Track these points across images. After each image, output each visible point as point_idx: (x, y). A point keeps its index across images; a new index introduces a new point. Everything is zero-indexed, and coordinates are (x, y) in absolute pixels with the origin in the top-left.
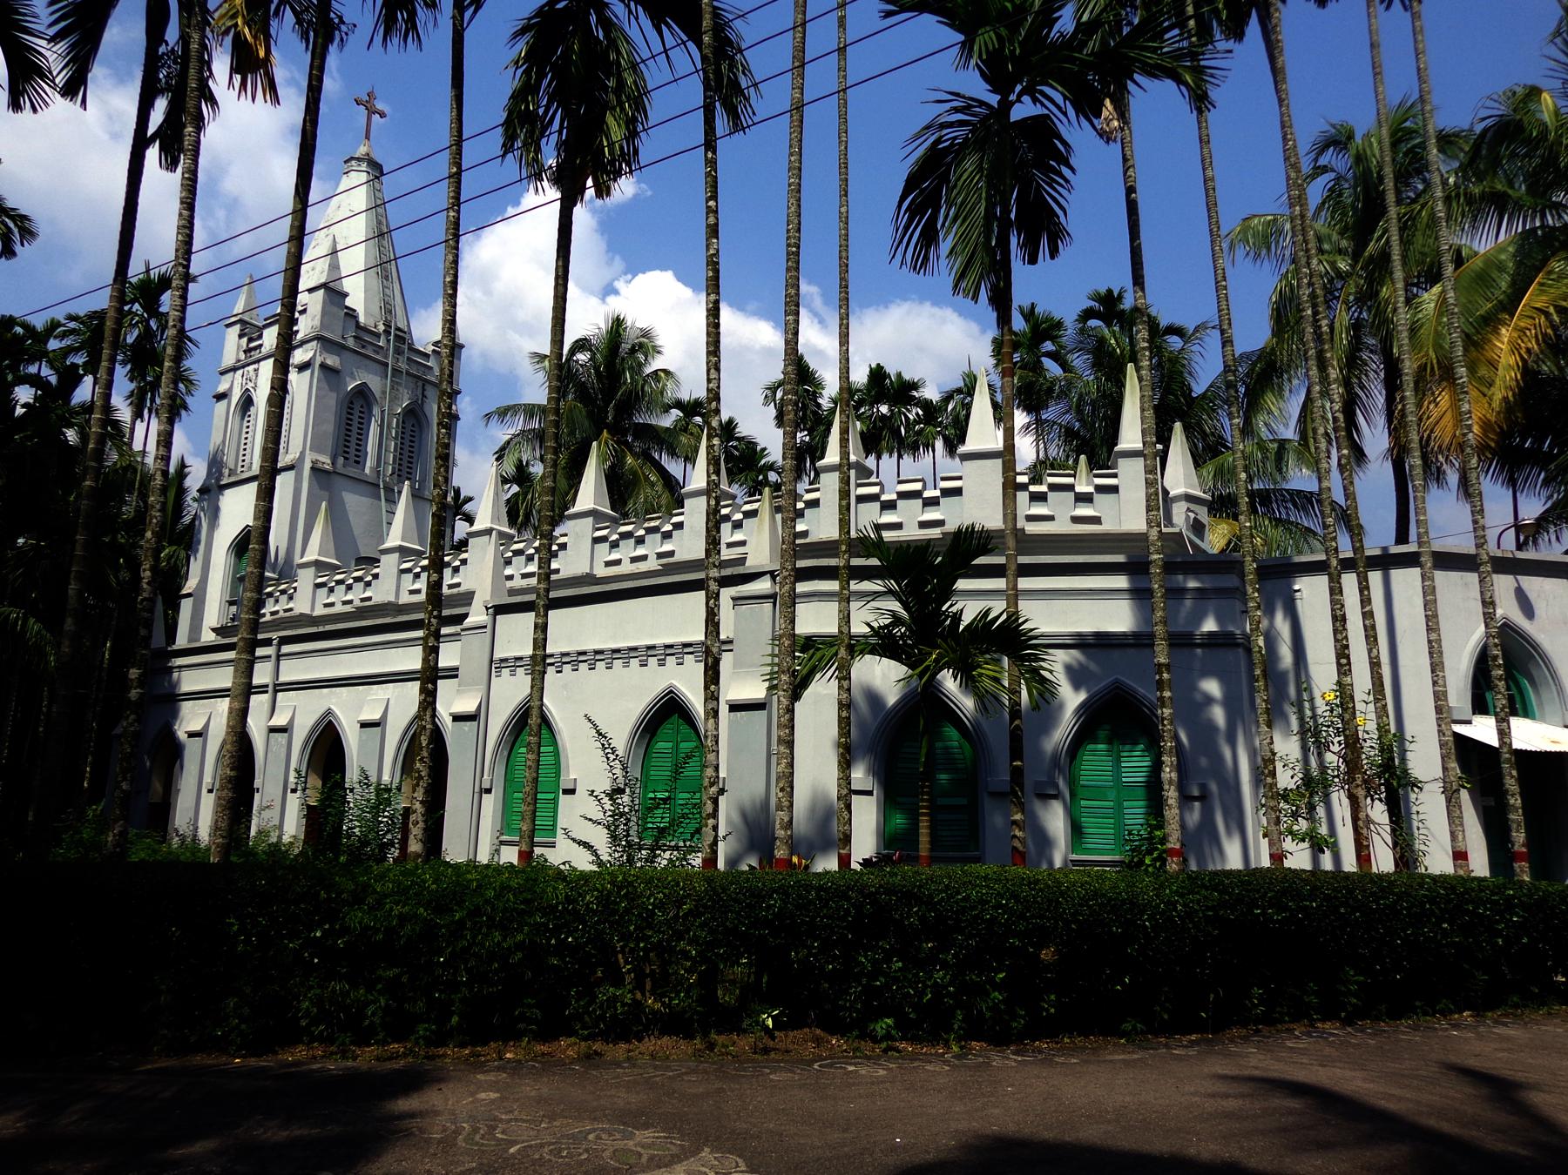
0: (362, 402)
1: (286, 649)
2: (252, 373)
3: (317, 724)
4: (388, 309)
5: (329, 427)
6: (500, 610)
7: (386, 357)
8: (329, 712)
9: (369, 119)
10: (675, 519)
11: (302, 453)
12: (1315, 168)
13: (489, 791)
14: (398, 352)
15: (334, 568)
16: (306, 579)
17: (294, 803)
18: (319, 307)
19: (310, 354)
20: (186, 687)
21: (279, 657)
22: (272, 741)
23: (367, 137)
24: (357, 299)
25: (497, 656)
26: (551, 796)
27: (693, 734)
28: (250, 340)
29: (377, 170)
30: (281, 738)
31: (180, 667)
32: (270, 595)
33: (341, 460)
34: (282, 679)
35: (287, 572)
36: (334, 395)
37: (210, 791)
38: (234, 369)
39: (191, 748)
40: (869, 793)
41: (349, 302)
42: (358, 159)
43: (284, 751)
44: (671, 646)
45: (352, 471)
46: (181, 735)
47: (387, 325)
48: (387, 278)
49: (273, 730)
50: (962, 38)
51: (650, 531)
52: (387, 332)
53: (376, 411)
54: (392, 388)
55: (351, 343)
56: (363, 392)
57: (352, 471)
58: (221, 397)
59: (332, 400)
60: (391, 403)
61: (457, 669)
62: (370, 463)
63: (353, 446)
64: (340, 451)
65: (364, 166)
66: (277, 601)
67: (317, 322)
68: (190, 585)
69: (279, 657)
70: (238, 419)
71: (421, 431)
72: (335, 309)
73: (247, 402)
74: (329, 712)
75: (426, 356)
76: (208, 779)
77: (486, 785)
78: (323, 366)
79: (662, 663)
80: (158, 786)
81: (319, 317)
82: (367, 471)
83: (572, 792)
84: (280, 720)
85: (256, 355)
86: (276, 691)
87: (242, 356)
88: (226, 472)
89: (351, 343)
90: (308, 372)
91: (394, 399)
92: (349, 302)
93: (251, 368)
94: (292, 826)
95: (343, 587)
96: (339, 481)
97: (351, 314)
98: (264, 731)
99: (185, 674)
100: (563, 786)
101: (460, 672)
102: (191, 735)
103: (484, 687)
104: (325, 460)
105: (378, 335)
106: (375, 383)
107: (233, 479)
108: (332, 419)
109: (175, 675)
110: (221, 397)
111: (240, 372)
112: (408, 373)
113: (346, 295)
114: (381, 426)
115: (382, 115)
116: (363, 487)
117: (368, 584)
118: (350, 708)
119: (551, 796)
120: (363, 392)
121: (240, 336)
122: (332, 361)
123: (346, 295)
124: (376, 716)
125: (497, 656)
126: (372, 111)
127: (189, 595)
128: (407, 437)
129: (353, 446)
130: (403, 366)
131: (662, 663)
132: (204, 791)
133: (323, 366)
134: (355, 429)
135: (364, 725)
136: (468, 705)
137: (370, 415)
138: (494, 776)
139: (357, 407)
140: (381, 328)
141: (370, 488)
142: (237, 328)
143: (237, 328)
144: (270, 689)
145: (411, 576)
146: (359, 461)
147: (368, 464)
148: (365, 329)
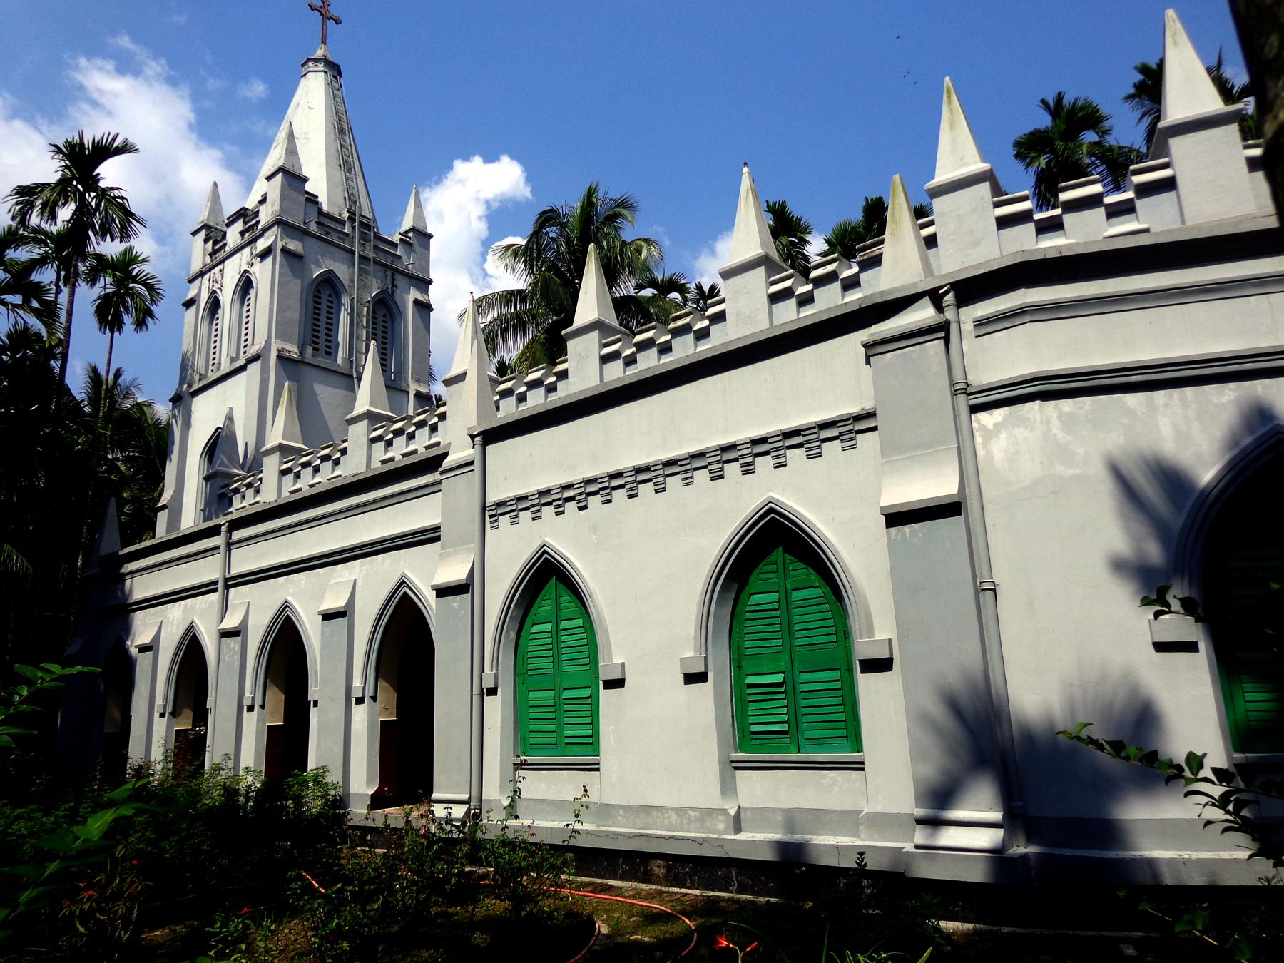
0: (329, 291)
1: (237, 535)
2: (218, 275)
3: (274, 621)
4: (352, 201)
5: (295, 314)
6: (491, 436)
7: (352, 244)
8: (286, 606)
9: (324, 24)
10: (711, 311)
11: (268, 342)
12: (247, 936)
13: (492, 692)
14: (364, 237)
15: (298, 452)
16: (271, 466)
17: (251, 723)
18: (278, 192)
19: (272, 240)
20: (138, 595)
21: (229, 546)
22: (224, 646)
23: (324, 42)
24: (318, 185)
25: (492, 498)
26: (586, 693)
27: (814, 577)
28: (215, 243)
29: (334, 69)
30: (234, 643)
31: (132, 572)
32: (236, 491)
33: (309, 350)
34: (235, 571)
35: (254, 466)
36: (299, 282)
37: (162, 715)
38: (201, 274)
39: (143, 663)
40: (1191, 647)
41: (309, 187)
42: (315, 60)
43: (237, 658)
44: (763, 440)
45: (322, 361)
46: (134, 651)
47: (352, 213)
48: (349, 170)
49: (225, 634)
50: (553, 580)
51: (677, 332)
52: (352, 219)
53: (345, 300)
54: (360, 275)
55: (313, 227)
56: (329, 280)
57: (322, 361)
58: (189, 303)
59: (296, 286)
60: (360, 290)
61: (438, 528)
62: (342, 353)
63: (323, 336)
64: (309, 339)
65: (321, 67)
66: (243, 497)
67: (277, 207)
68: (166, 498)
69: (229, 546)
70: (206, 323)
71: (393, 322)
72: (295, 194)
73: (214, 305)
74: (286, 606)
75: (394, 245)
76: (159, 701)
77: (489, 683)
78: (285, 250)
79: (748, 470)
80: (116, 714)
81: (278, 202)
82: (339, 361)
83: (618, 684)
84: (231, 622)
85: (220, 255)
86: (227, 587)
87: (208, 260)
88: (197, 378)
89: (313, 227)
90: (270, 259)
91: (364, 287)
92: (309, 187)
93: (217, 270)
94: (251, 756)
95: (310, 470)
96: (309, 373)
97: (312, 199)
98: (216, 636)
99: (138, 580)
100: (604, 675)
101: (443, 533)
102: (143, 649)
103: (476, 545)
104: (293, 350)
105: (342, 223)
106: (342, 271)
107: (203, 383)
108: (298, 305)
109: (128, 582)
110: (189, 303)
111: (207, 276)
112: (376, 262)
113: (305, 180)
114: (351, 314)
115: (338, 22)
116: (336, 378)
117: (337, 462)
118: (308, 598)
119: (586, 693)
120: (329, 280)
121: (206, 241)
122: (293, 245)
123: (305, 180)
124: (339, 603)
125: (492, 498)
126: (327, 17)
127: (164, 507)
128: (380, 324)
129: (323, 336)
130: (371, 254)
131: (748, 470)
132: (156, 715)
133: (285, 250)
134: (323, 318)
135: (327, 616)
136: (455, 572)
137: (339, 304)
138: (498, 669)
139: (325, 297)
140: (346, 215)
141: (342, 380)
142: (202, 234)
143: (202, 234)
144: (220, 586)
145: (382, 445)
146: (331, 351)
147: (340, 354)
148: (328, 216)
